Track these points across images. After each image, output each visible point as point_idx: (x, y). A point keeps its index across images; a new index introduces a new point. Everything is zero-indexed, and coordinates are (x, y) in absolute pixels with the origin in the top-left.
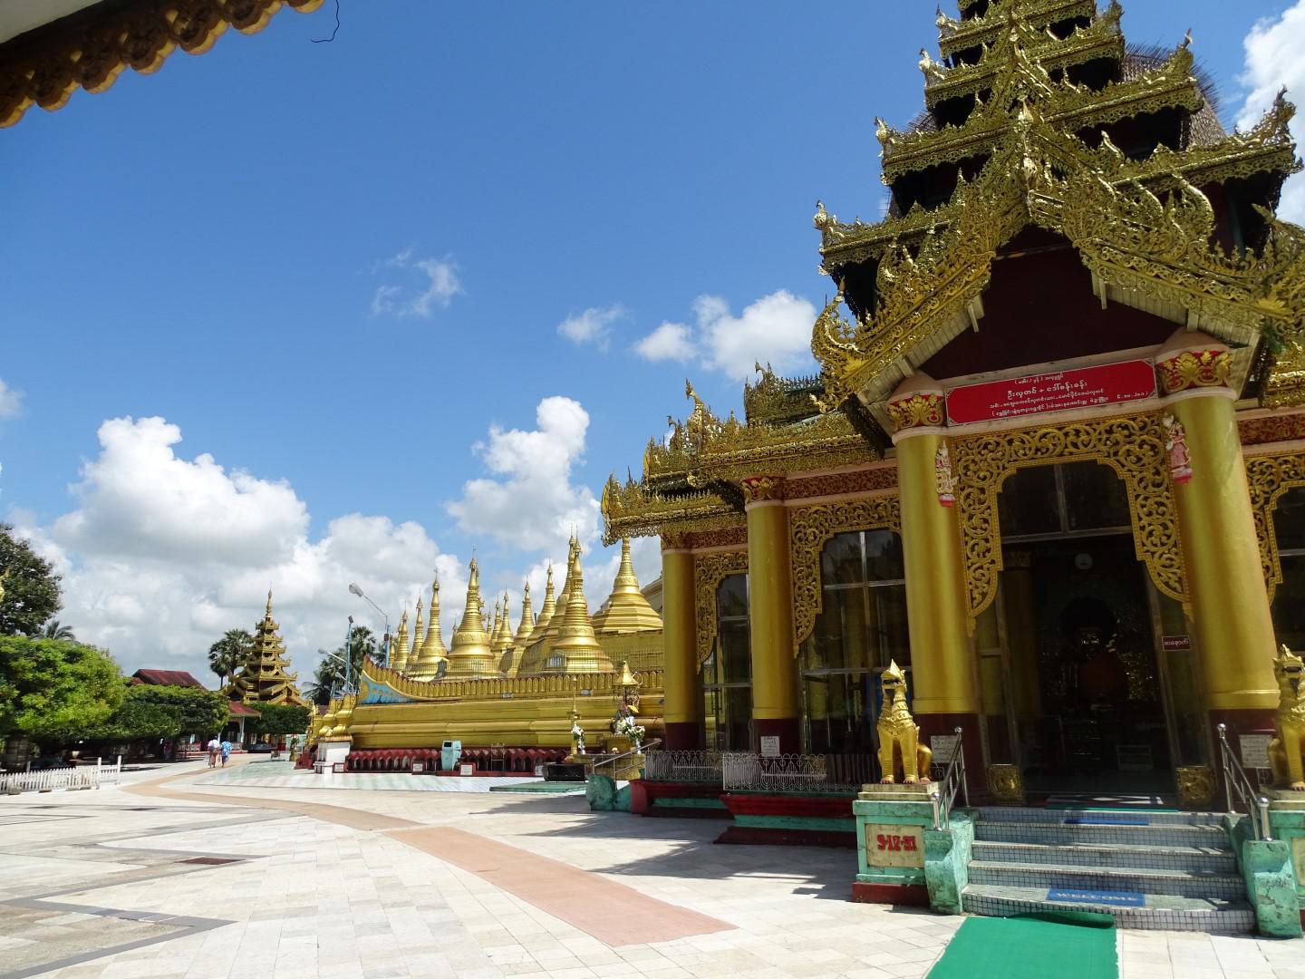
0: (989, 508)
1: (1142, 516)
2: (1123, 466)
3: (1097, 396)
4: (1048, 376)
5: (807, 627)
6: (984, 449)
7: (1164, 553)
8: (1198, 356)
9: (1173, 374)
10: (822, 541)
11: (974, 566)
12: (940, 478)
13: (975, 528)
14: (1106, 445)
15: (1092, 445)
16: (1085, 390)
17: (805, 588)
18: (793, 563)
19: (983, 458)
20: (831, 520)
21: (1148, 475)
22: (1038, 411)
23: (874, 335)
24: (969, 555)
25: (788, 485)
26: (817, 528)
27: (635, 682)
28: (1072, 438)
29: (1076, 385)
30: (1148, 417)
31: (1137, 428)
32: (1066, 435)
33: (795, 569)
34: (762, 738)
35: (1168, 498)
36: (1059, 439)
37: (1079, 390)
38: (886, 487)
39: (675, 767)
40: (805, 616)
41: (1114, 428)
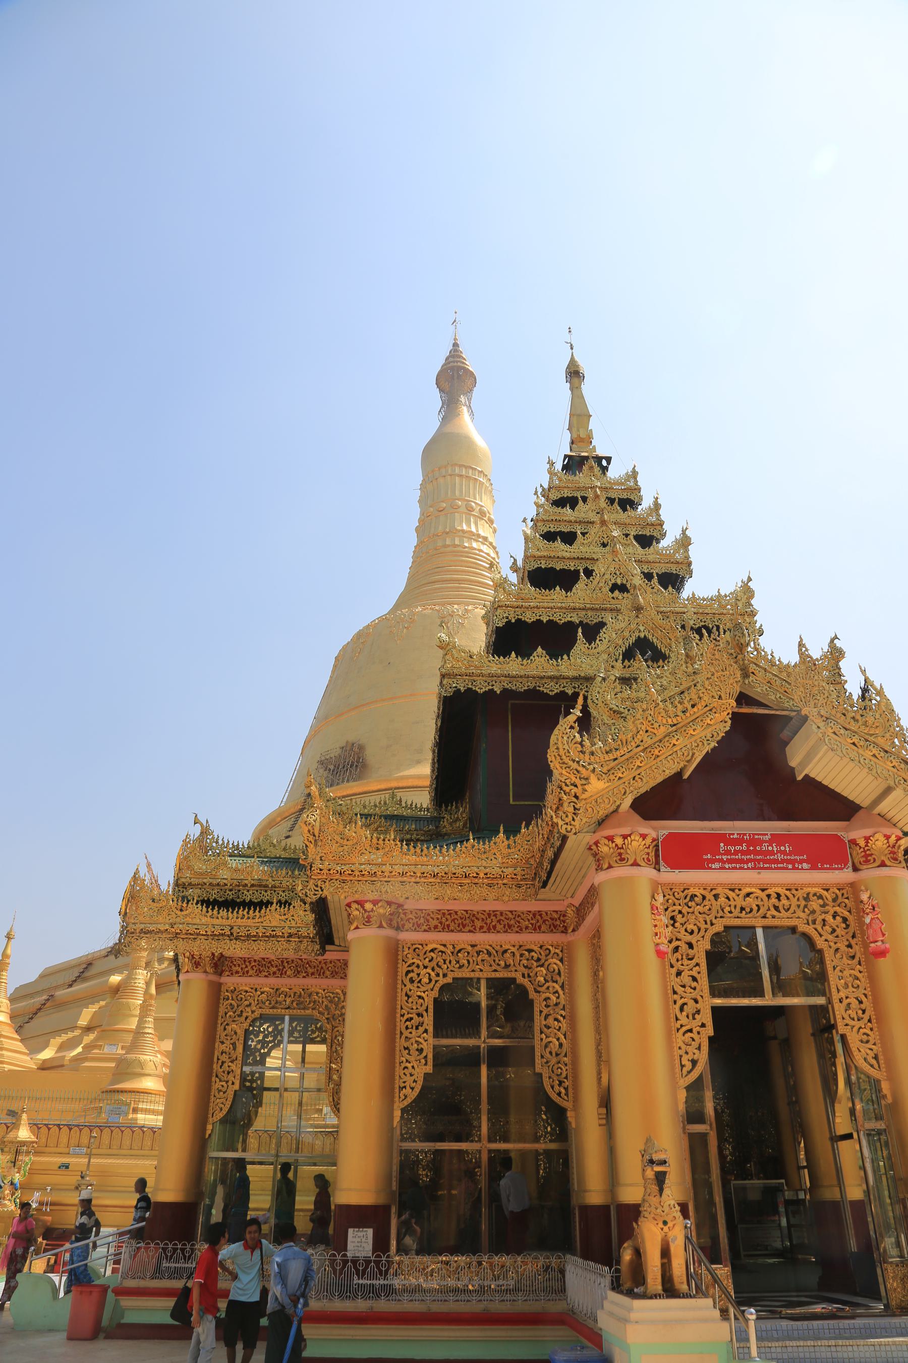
0: (697, 964)
1: (840, 988)
2: (821, 936)
3: (801, 862)
4: (758, 834)
5: (412, 1089)
6: (690, 900)
7: (860, 1028)
8: (888, 837)
9: (865, 851)
10: (438, 985)
11: (684, 1029)
12: (656, 926)
13: (684, 986)
14: (804, 912)
15: (791, 910)
16: (790, 854)
17: (413, 1040)
18: (402, 1008)
19: (690, 910)
20: (450, 962)
21: (842, 946)
22: (748, 868)
23: (616, 759)
24: (679, 1016)
25: (405, 914)
26: (433, 970)
27: (33, 1138)
28: (773, 900)
29: (782, 848)
30: (839, 889)
31: (830, 899)
32: (769, 896)
33: (402, 1016)
34: (350, 1231)
35: (860, 972)
36: (762, 900)
37: (784, 853)
38: (517, 932)
39: (165, 1264)
40: (411, 1075)
41: (811, 895)
